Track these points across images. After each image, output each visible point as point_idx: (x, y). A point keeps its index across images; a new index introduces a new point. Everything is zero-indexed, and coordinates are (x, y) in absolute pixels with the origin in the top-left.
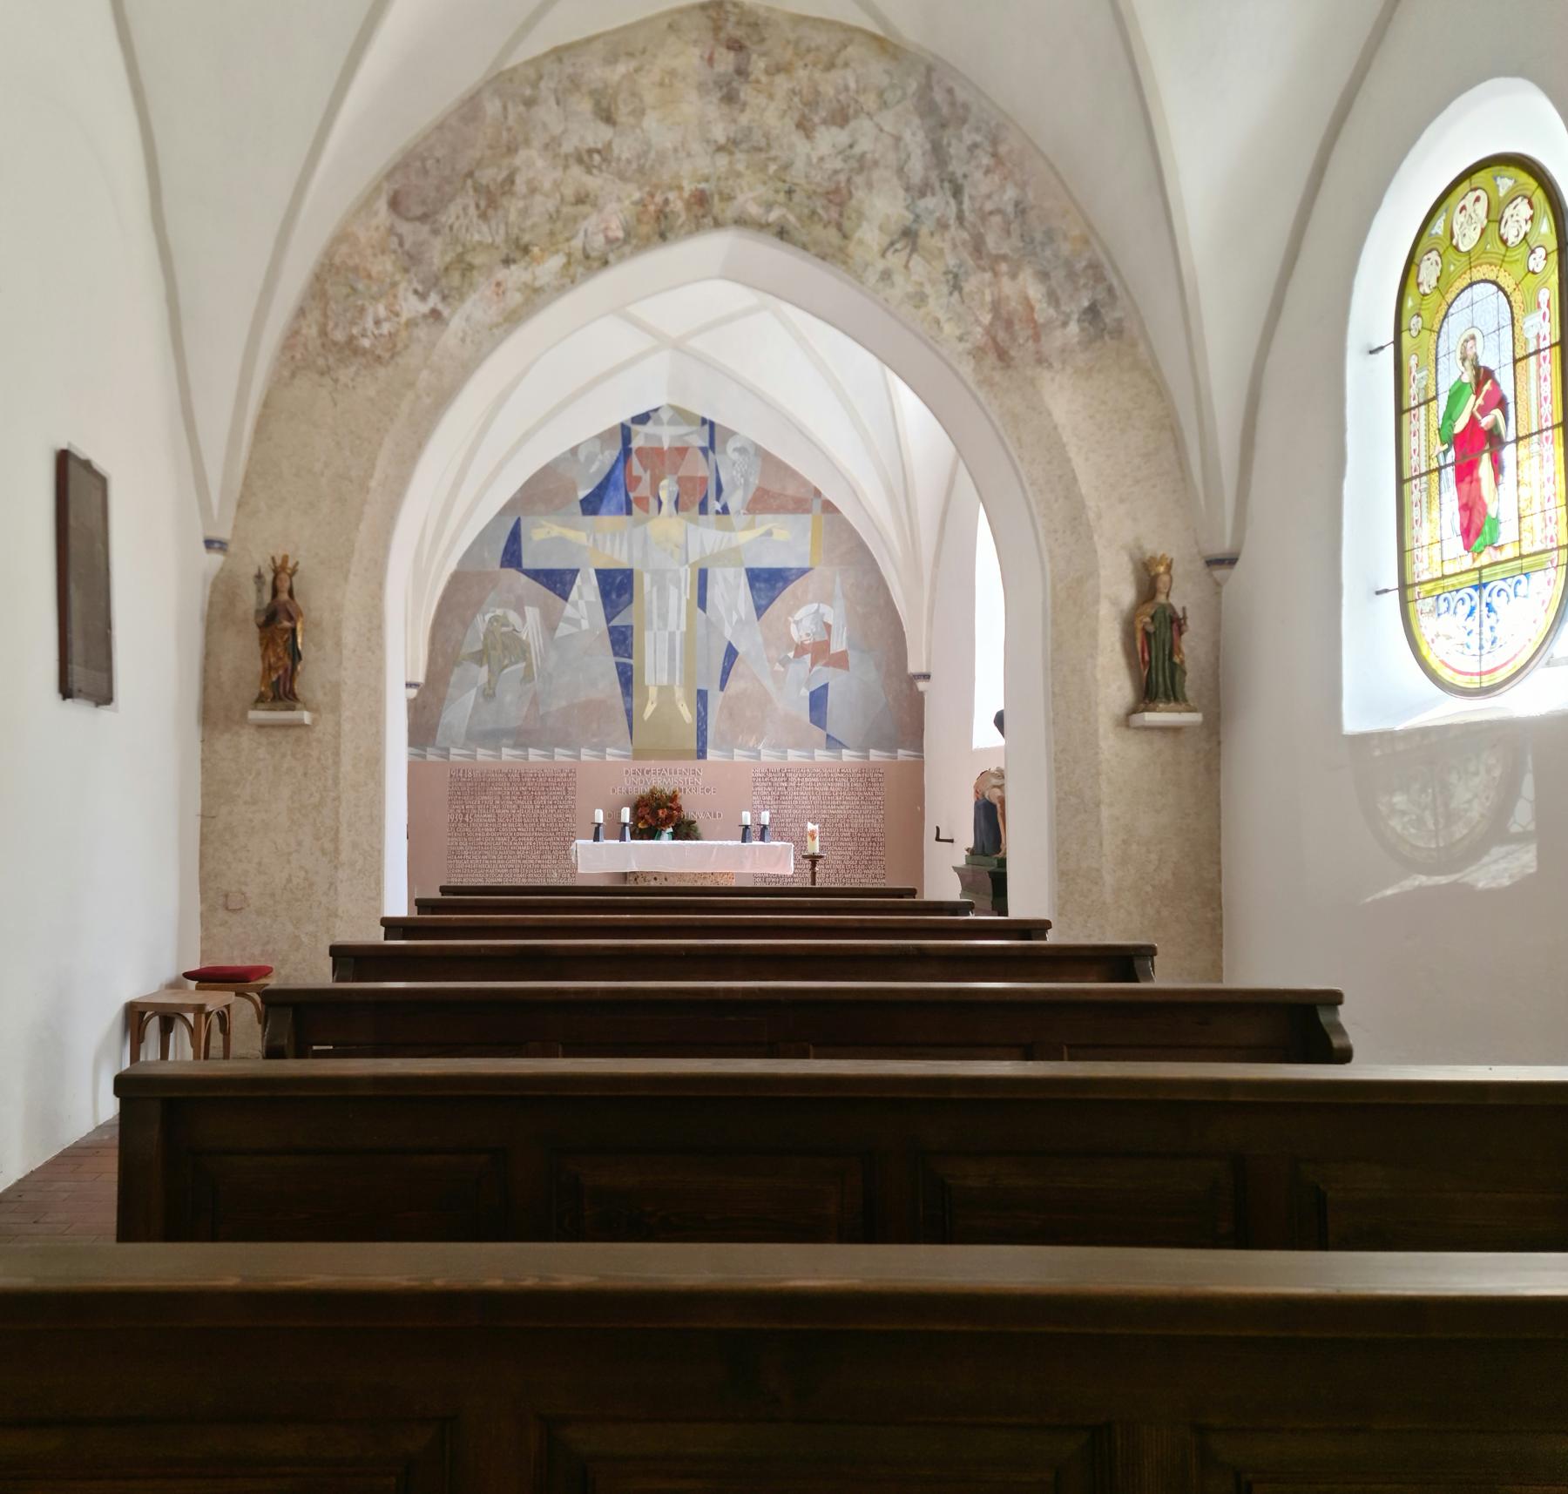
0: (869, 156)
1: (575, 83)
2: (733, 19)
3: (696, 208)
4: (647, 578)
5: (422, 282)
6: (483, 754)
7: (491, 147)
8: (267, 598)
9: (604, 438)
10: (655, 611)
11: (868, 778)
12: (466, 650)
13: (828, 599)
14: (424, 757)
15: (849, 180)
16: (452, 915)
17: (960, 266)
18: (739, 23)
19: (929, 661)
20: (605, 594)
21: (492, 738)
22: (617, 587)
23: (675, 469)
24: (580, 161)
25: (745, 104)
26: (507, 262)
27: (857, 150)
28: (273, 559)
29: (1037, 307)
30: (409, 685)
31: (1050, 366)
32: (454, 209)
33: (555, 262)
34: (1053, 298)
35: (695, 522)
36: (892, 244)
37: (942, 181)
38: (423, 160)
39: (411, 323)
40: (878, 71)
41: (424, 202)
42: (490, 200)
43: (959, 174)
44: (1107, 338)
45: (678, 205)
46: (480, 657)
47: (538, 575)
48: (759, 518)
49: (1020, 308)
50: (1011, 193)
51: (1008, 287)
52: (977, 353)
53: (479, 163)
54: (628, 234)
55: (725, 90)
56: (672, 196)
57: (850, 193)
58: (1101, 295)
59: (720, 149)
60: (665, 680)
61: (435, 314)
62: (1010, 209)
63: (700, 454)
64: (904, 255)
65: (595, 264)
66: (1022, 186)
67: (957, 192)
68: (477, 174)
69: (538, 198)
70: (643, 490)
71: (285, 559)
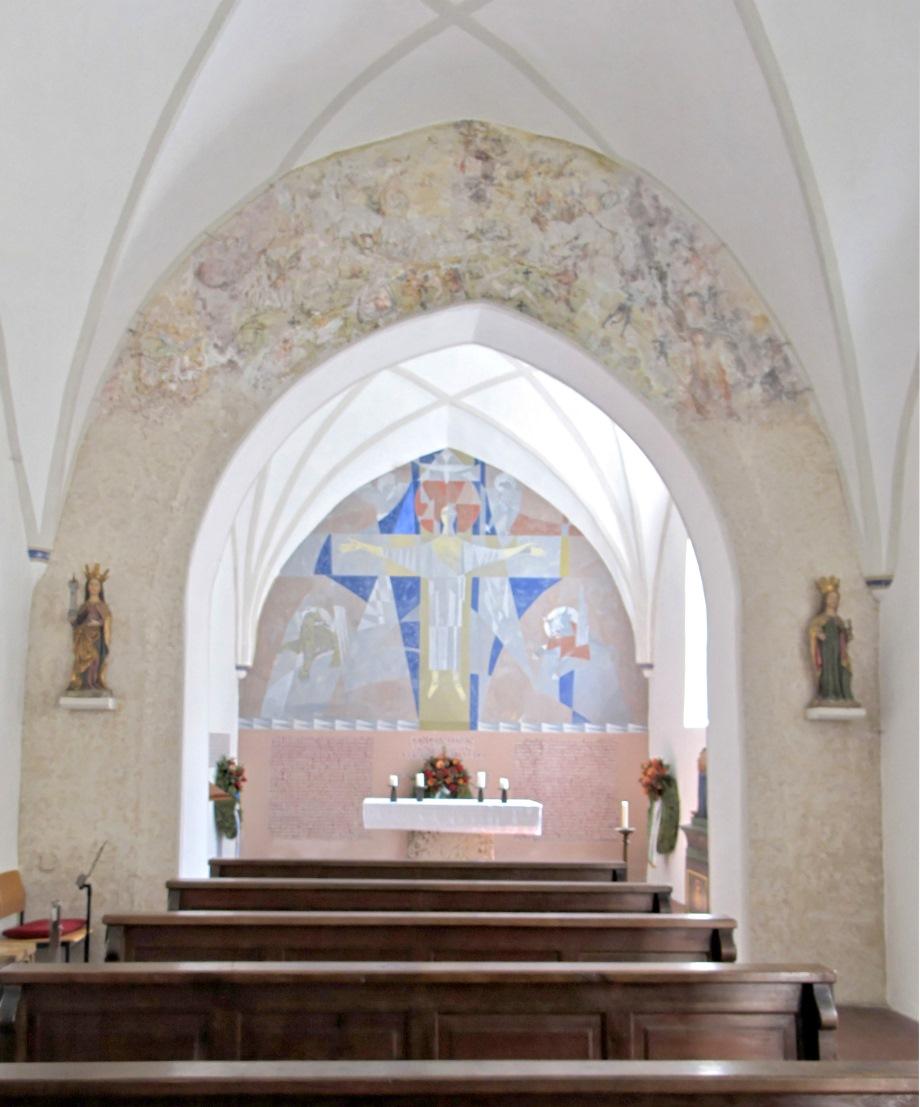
0: (590, 247)
1: (351, 181)
2: (480, 135)
3: (451, 284)
4: (431, 586)
5: (221, 338)
6: (298, 725)
7: (281, 231)
8: (81, 600)
9: (398, 471)
10: (437, 613)
11: (605, 745)
12: (286, 640)
13: (573, 604)
14: (250, 726)
15: (575, 265)
16: (235, 882)
17: (665, 336)
18: (485, 139)
19: (652, 654)
20: (398, 597)
21: (306, 711)
22: (407, 590)
23: (454, 498)
24: (355, 243)
25: (491, 202)
26: (293, 323)
27: (581, 242)
28: (87, 567)
29: (728, 370)
30: (239, 668)
31: (739, 419)
32: (249, 279)
33: (334, 325)
34: (740, 364)
35: (469, 541)
36: (611, 316)
37: (650, 268)
38: (225, 239)
39: (211, 372)
40: (597, 180)
41: (224, 273)
42: (279, 274)
43: (663, 264)
44: (784, 398)
45: (435, 281)
46: (297, 646)
47: (343, 580)
48: (520, 538)
49: (714, 372)
50: (705, 281)
51: (705, 355)
52: (680, 407)
53: (272, 243)
54: (394, 302)
55: (474, 190)
56: (430, 273)
57: (576, 275)
58: (779, 363)
59: (470, 237)
60: (445, 667)
61: (231, 363)
62: (705, 293)
63: (473, 487)
64: (620, 326)
65: (368, 327)
66: (715, 274)
67: (662, 277)
68: (269, 252)
69: (320, 272)
70: (429, 514)
71: (97, 567)
